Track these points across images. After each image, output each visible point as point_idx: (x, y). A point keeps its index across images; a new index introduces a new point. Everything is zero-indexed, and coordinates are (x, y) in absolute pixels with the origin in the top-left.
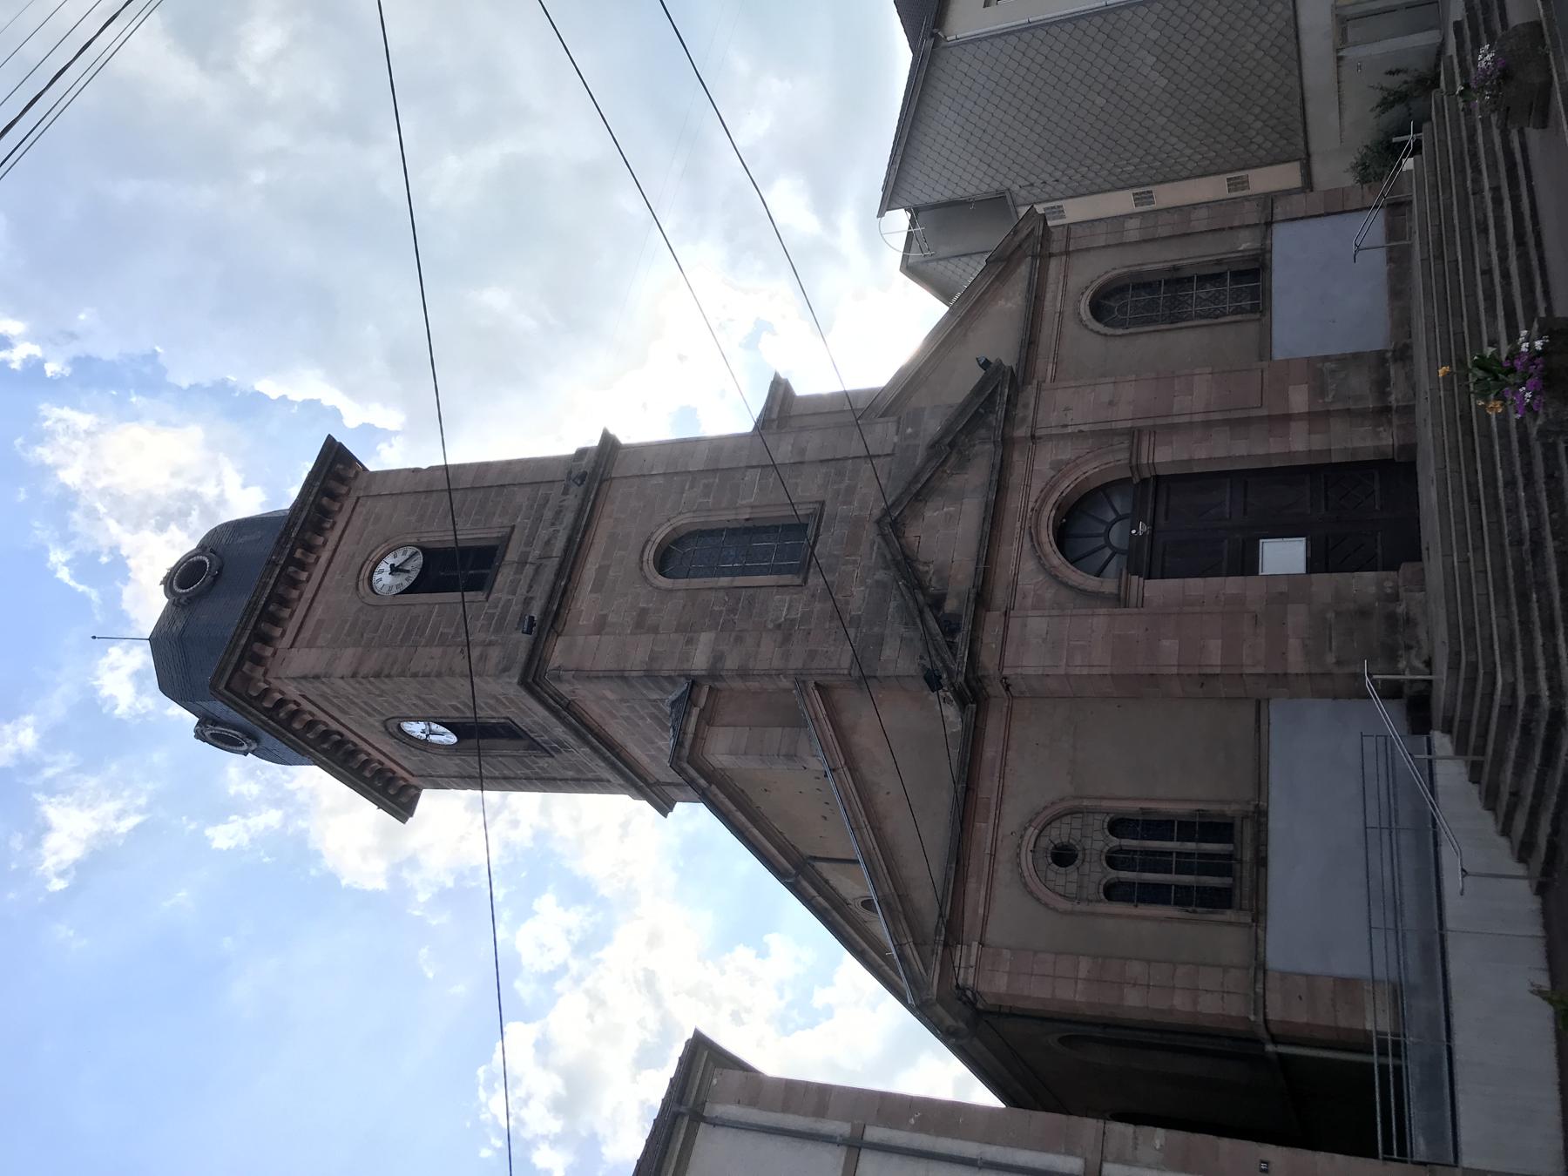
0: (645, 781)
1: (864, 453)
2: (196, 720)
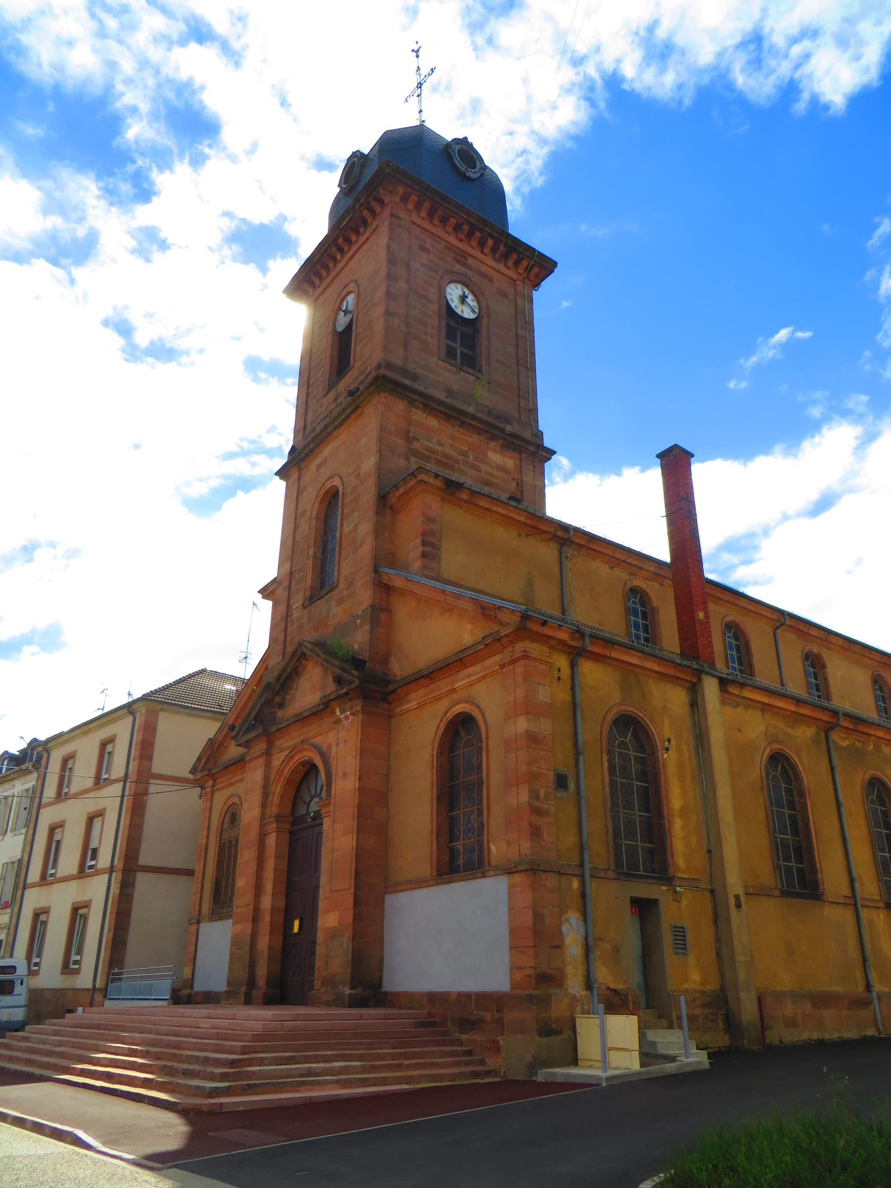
0: (303, 459)
1: (569, 551)
2: (366, 153)
